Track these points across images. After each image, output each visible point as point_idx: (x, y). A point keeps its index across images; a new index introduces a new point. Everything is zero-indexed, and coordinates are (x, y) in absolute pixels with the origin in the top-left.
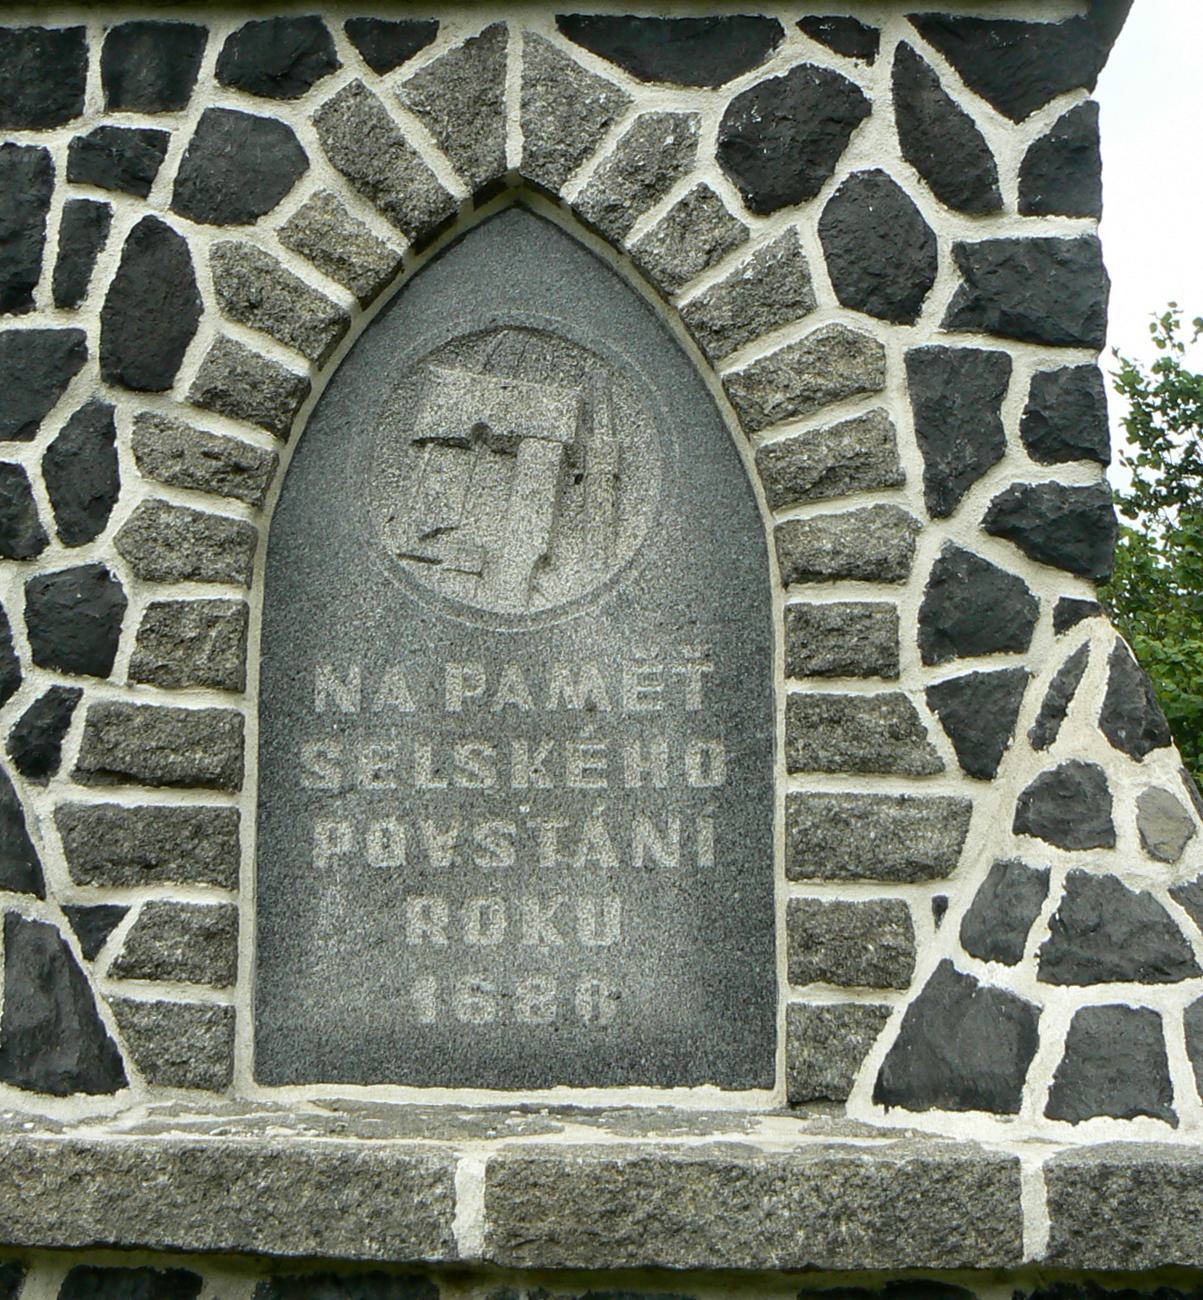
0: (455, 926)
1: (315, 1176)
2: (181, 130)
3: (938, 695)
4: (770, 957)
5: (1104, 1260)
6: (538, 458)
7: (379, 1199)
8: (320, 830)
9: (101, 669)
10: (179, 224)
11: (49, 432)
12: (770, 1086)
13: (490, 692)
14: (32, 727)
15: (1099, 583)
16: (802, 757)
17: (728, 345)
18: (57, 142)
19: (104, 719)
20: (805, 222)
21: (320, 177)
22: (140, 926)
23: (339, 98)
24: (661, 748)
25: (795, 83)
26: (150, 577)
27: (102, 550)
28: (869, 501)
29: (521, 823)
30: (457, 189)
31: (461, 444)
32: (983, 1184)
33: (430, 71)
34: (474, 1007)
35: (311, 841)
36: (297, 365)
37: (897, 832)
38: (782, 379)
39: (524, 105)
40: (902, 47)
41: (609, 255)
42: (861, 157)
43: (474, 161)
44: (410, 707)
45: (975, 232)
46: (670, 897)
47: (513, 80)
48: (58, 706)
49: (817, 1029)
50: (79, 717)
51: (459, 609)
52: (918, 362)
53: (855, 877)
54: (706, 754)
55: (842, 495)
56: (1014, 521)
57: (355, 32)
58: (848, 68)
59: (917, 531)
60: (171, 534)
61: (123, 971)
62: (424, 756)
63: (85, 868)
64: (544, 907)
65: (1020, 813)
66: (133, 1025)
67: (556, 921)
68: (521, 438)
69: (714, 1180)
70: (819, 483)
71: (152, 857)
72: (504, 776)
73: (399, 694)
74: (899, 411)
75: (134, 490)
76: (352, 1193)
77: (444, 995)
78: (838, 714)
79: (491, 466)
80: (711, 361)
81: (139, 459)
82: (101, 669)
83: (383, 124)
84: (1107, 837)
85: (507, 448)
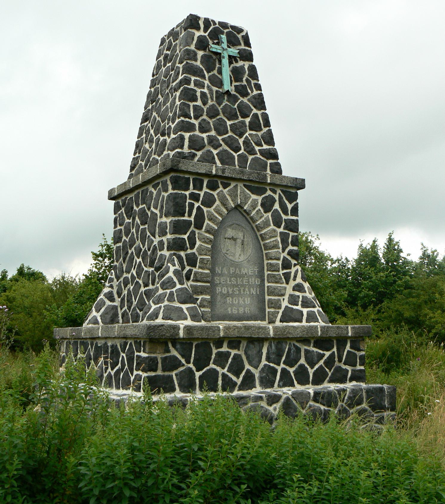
0: (232, 301)
2: (202, 194)
6: (239, 241)
8: (217, 288)
9: (195, 267)
10: (202, 207)
11: (188, 234)
13: (235, 271)
18: (187, 193)
19: (196, 273)
20: (270, 214)
21: (218, 203)
23: (220, 192)
24: (253, 279)
26: (201, 255)
27: (194, 250)
28: (276, 250)
30: (233, 206)
31: (230, 239)
34: (235, 312)
37: (280, 291)
41: (248, 217)
44: (226, 273)
46: (255, 297)
50: (193, 273)
51: (232, 261)
52: (281, 233)
53: (276, 296)
57: (221, 183)
62: (228, 279)
65: (293, 289)
67: (243, 301)
70: (273, 247)
72: (237, 282)
73: (225, 271)
74: (279, 239)
75: (198, 243)
76: (260, 330)
77: (231, 310)
78: (274, 276)
79: (233, 242)
82: (195, 267)
84: (305, 292)
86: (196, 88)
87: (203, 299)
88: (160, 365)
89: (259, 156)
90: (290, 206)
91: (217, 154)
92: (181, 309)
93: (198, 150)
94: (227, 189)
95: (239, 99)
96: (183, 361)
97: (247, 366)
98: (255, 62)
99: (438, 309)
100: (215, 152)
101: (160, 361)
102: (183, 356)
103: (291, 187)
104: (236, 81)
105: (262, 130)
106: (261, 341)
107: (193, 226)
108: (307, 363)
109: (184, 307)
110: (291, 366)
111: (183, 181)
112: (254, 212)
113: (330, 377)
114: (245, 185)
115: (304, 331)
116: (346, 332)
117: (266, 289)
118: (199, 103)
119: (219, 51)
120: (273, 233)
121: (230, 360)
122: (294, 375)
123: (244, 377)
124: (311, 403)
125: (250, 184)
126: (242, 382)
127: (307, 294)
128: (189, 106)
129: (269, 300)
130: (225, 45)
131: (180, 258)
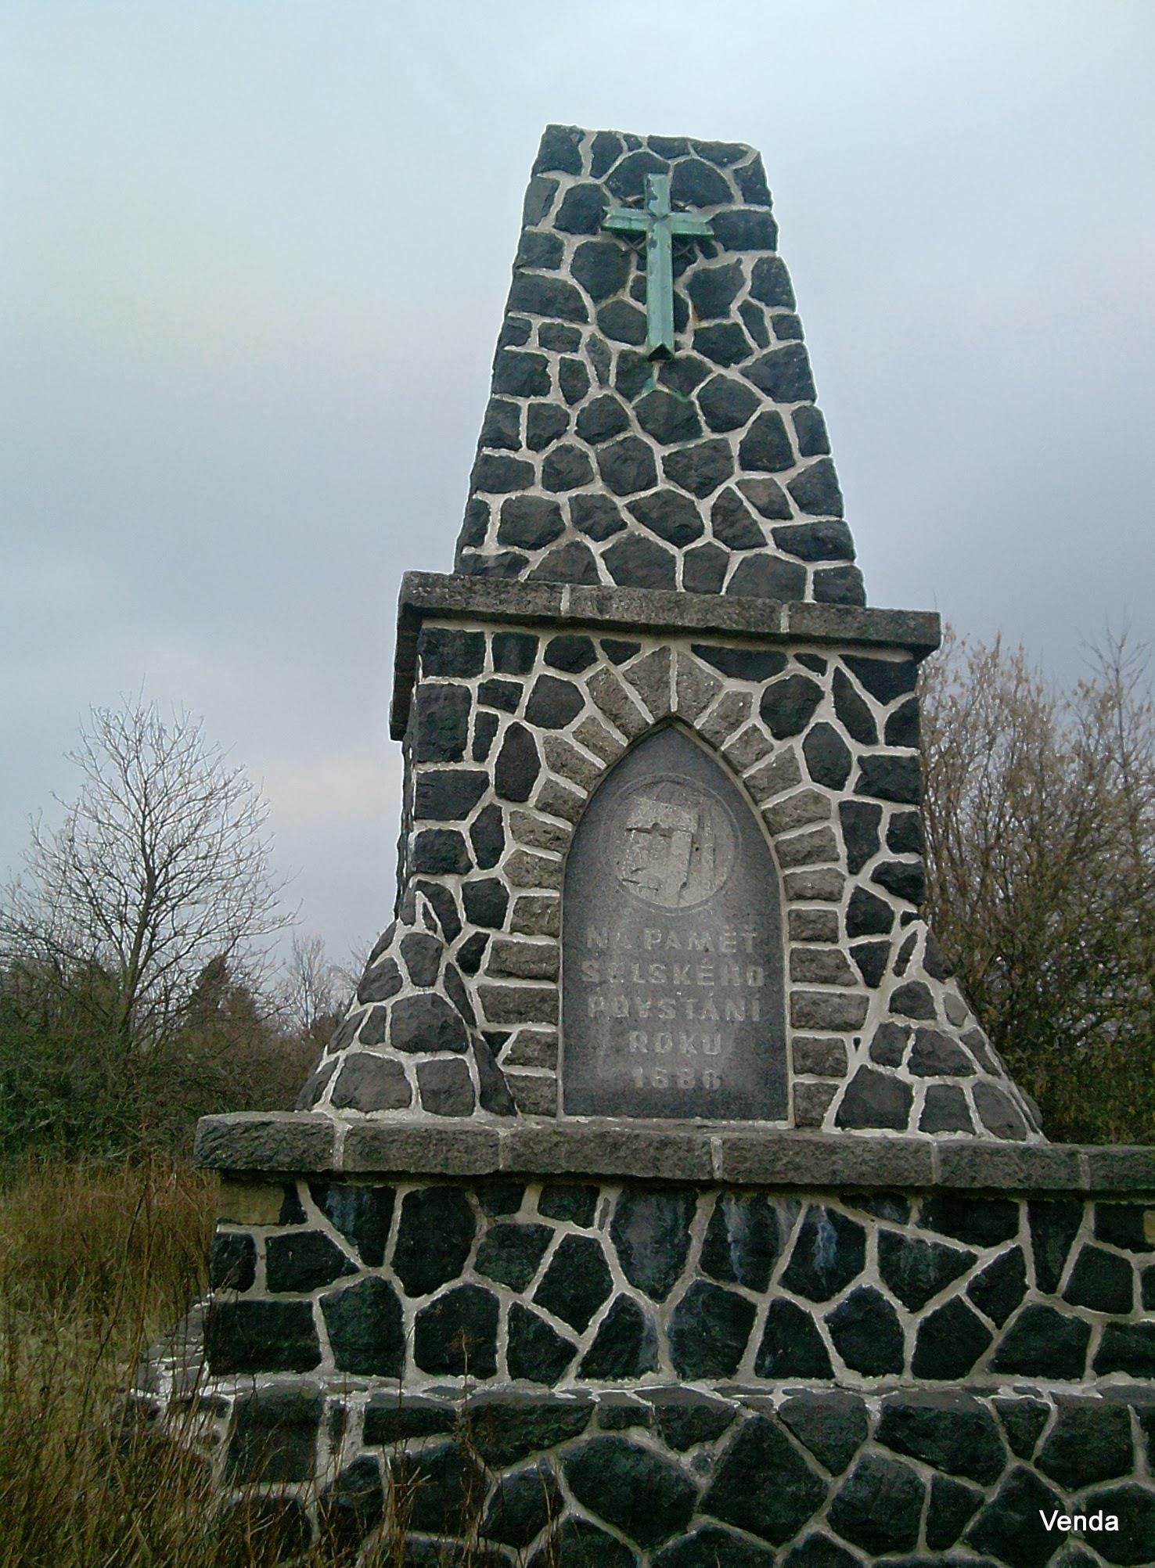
1: (655, 1144)
2: (529, 683)
3: (854, 951)
4: (784, 1063)
5: (961, 1184)
6: (680, 842)
7: (681, 1153)
8: (591, 1000)
9: (499, 926)
10: (528, 726)
11: (472, 817)
12: (786, 1119)
13: (663, 942)
14: (468, 951)
15: (918, 905)
16: (799, 975)
17: (766, 795)
18: (473, 685)
19: (498, 949)
20: (797, 743)
21: (590, 710)
22: (517, 1041)
25: (793, 682)
26: (518, 885)
27: (497, 872)
29: (677, 999)
30: (651, 720)
32: (917, 1151)
33: (639, 665)
34: (659, 1079)
35: (587, 1005)
36: (583, 794)
37: (839, 1009)
38: (788, 811)
39: (677, 684)
40: (837, 670)
42: (820, 716)
43: (657, 708)
45: (866, 751)
47: (673, 674)
48: (479, 941)
49: (809, 1093)
50: (489, 945)
52: (844, 807)
53: (822, 1028)
54: (755, 972)
55: (814, 863)
56: (883, 877)
58: (814, 677)
59: (844, 880)
60: (529, 867)
61: (509, 1061)
63: (492, 1015)
64: (688, 1037)
66: (515, 1086)
68: (673, 830)
69: (812, 1148)
71: (523, 1010)
72: (670, 979)
78: (814, 957)
80: (756, 802)
81: (513, 832)
82: (499, 926)
83: (618, 689)
84: (932, 1015)
85: (667, 834)
86: (544, 352)
87: (526, 1038)
88: (261, 1268)
89: (771, 549)
90: (881, 713)
91: (603, 555)
92: (399, 1071)
93: (535, 546)
94: (626, 666)
95: (710, 371)
96: (353, 1255)
97: (621, 1285)
98: (783, 251)
99: (677, 1245)
100: (597, 548)
101: (261, 1249)
102: (353, 1236)
103: (880, 645)
104: (702, 315)
105: (793, 464)
106: (687, 1190)
107: (491, 789)
108: (891, 1289)
109: (410, 1062)
110: (820, 1297)
111: (458, 643)
112: (730, 741)
113: (1000, 1351)
114: (696, 650)
115: (864, 1162)
116: (1063, 1173)
117: (787, 1001)
118: (555, 397)
119: (637, 226)
120: (812, 808)
121: (548, 1259)
122: (832, 1332)
123: (605, 1327)
124: (874, 1450)
125: (718, 645)
126: (595, 1346)
127: (943, 1024)
128: (517, 409)
129: (796, 1041)
130: (660, 204)
131: (438, 896)
